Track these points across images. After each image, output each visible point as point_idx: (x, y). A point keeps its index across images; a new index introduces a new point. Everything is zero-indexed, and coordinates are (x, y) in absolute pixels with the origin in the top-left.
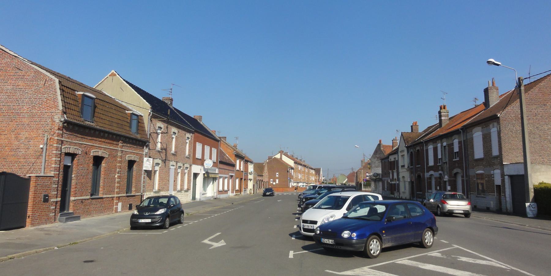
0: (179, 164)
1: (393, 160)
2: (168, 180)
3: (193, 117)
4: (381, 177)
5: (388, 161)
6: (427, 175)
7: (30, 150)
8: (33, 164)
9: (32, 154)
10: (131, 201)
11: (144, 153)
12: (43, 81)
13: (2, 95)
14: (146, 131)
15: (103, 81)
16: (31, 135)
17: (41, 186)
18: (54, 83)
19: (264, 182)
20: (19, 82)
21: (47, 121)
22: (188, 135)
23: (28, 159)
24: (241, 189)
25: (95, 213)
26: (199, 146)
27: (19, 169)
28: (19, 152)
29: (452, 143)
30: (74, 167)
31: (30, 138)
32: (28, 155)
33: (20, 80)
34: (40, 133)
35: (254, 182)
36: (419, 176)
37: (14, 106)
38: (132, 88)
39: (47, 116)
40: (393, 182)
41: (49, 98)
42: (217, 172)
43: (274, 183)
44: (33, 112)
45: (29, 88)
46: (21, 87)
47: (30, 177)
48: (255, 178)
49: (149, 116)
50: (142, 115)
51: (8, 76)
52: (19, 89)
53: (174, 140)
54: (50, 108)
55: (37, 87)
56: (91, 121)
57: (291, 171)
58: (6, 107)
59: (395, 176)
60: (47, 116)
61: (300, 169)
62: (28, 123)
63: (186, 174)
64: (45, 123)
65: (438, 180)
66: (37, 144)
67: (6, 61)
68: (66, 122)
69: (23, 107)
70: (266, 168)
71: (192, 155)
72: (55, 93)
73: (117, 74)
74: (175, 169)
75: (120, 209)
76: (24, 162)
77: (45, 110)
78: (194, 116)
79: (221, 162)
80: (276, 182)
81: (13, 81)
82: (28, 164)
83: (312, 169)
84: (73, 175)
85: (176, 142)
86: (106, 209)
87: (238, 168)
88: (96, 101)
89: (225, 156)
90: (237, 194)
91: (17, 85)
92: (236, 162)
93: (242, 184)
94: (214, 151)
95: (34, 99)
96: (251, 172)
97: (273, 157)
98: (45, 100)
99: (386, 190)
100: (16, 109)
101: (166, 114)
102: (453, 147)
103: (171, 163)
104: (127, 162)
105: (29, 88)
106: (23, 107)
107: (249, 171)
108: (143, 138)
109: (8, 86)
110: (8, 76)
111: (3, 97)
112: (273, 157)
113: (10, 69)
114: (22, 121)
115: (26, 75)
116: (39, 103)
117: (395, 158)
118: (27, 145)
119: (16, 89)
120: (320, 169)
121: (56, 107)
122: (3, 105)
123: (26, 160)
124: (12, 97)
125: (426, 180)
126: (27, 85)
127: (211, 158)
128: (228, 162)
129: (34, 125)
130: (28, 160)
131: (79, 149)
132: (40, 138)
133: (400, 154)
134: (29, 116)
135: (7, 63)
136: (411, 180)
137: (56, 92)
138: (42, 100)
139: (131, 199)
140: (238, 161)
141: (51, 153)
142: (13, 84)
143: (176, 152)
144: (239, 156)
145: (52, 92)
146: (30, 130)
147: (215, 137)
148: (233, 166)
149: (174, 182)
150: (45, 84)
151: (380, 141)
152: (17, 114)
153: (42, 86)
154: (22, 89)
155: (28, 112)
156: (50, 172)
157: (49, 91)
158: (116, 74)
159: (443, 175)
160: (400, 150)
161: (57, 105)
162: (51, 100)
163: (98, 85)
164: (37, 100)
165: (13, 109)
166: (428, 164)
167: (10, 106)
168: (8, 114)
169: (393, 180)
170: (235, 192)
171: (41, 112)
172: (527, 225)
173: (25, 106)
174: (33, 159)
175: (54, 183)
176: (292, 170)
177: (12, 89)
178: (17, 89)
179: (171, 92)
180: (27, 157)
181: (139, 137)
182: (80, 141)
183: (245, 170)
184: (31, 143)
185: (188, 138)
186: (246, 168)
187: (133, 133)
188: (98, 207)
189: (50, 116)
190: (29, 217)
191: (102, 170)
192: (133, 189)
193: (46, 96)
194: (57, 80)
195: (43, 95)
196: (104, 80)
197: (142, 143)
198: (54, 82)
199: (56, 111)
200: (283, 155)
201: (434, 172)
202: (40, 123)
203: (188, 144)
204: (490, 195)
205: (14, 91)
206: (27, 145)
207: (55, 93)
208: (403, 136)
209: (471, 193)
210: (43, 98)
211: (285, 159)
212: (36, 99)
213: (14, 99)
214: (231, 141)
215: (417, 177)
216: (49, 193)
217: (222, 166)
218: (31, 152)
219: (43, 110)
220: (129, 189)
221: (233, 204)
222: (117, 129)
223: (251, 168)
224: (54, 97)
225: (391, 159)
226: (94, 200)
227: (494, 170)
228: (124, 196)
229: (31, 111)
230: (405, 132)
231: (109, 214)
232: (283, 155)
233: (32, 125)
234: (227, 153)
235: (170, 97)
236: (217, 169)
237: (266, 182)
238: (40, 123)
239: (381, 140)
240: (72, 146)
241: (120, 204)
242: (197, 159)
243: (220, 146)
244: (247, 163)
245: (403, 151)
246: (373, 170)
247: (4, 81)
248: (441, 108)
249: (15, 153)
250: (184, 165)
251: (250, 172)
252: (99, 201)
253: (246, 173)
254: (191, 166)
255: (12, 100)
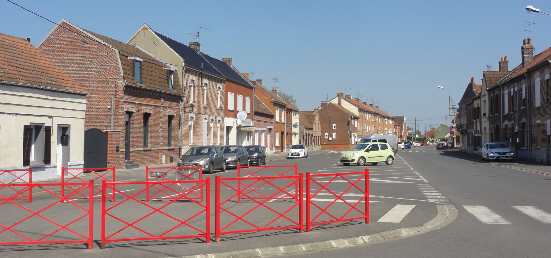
0: (212, 117)
1: (476, 106)
2: (202, 135)
3: (221, 60)
4: (465, 129)
5: (473, 107)
6: (503, 125)
7: (100, 110)
8: (104, 121)
9: (102, 113)
10: (174, 154)
11: (180, 108)
12: (105, 52)
13: (73, 65)
14: (180, 86)
15: (135, 36)
16: (100, 97)
17: (115, 139)
18: (115, 53)
19: (315, 137)
20: (86, 53)
21: (111, 86)
22: (219, 85)
23: (99, 117)
24: (282, 146)
25: (147, 163)
26: (231, 96)
27: (93, 125)
28: (91, 112)
29: (521, 88)
30: (131, 123)
31: (99, 100)
32: (99, 114)
33: (87, 52)
34: (107, 96)
35: (300, 137)
36: (497, 127)
37: (84, 73)
38: (165, 42)
39: (112, 81)
40: (477, 135)
41: (112, 66)
42: (252, 125)
43: (330, 139)
44: (100, 79)
45: (95, 59)
46: (88, 57)
47: (107, 132)
48: (301, 132)
49: (183, 70)
50: (177, 69)
51: (77, 48)
52: (87, 59)
53: (206, 91)
54: (113, 75)
55: (102, 57)
56: (140, 82)
57: (354, 122)
58: (77, 75)
59: (479, 129)
60: (112, 81)
61: (367, 119)
62: (97, 88)
63: (219, 129)
64: (110, 88)
65: (511, 131)
66: (106, 105)
67: (74, 35)
68: (127, 87)
69: (91, 75)
70: (317, 119)
71: (224, 107)
72: (116, 62)
73: (148, 28)
74: (208, 122)
75: (164, 161)
76: (96, 120)
77: (109, 76)
78: (223, 59)
79: (256, 113)
80: (332, 137)
81: (81, 52)
82: (100, 121)
83: (389, 118)
84: (131, 130)
85: (207, 94)
86: (154, 160)
87: (277, 119)
88: (143, 63)
89: (261, 105)
90: (277, 151)
91: (85, 56)
92: (275, 112)
93: (283, 139)
94: (248, 100)
95: (100, 67)
96: (296, 124)
97: (328, 103)
98: (109, 68)
99: (471, 145)
100: (86, 76)
101: (198, 67)
102: (521, 93)
103: (204, 116)
104: (167, 116)
105: (95, 59)
106: (91, 75)
107: (293, 122)
108: (180, 94)
109: (77, 56)
110: (77, 48)
111: (74, 66)
112: (328, 103)
113: (78, 42)
114: (92, 86)
115: (91, 47)
116: (104, 71)
117: (478, 104)
118: (98, 106)
119: (84, 59)
120: (404, 117)
121: (119, 74)
122: (74, 73)
123: (98, 118)
124: (82, 66)
125: (502, 132)
126: (93, 56)
127: (244, 109)
128: (265, 112)
129: (102, 89)
130: (100, 118)
131: (135, 107)
132: (107, 100)
133: (483, 99)
134: (96, 82)
135: (75, 37)
136: (491, 132)
137: (118, 61)
138: (107, 68)
139: (172, 152)
140: (277, 112)
141: (117, 112)
142: (81, 55)
143: (207, 104)
144: (278, 105)
145: (114, 61)
146: (99, 93)
147: (248, 83)
148: (272, 117)
149: (208, 136)
150: (107, 54)
151: (472, 80)
152: (87, 80)
153: (106, 56)
154: (89, 59)
155: (96, 79)
156: (118, 128)
157: (112, 61)
158: (147, 28)
159: (514, 125)
160: (482, 94)
161: (119, 72)
162: (114, 68)
163: (131, 40)
164: (102, 68)
165: (84, 76)
166: (504, 112)
167: (81, 73)
168: (79, 81)
169: (476, 132)
170: (274, 148)
171: (107, 79)
172: (532, 171)
173: (93, 73)
174: (103, 117)
175: (121, 136)
176: (356, 122)
177: (81, 59)
178: (85, 59)
179: (198, 36)
180: (98, 116)
181: (175, 92)
182: (134, 101)
183: (287, 121)
184: (100, 104)
185: (220, 88)
186: (289, 119)
187: (170, 90)
188: (149, 158)
189: (114, 81)
190: (109, 162)
191: (149, 125)
192: (173, 143)
193: (109, 64)
194: (117, 51)
195: (107, 64)
196: (137, 34)
197: (178, 99)
198: (115, 52)
199: (118, 77)
200: (342, 99)
201: (508, 122)
202: (106, 88)
203: (219, 95)
204: (544, 146)
205: (83, 61)
206: (98, 106)
207: (116, 62)
208: (485, 76)
209: (533, 145)
210: (107, 67)
211: (346, 105)
212: (101, 67)
213: (83, 68)
214: (268, 85)
215: (495, 128)
216: (119, 145)
217: (257, 117)
218: (101, 111)
219: (108, 77)
220: (169, 144)
221: (271, 161)
222: (158, 87)
223: (295, 119)
224: (116, 65)
225: (475, 105)
226: (145, 152)
227: (546, 120)
228: (166, 149)
229: (98, 77)
230: (492, 71)
231: (157, 165)
232: (342, 99)
233: (100, 89)
234: (263, 101)
235: (197, 41)
236: (252, 121)
237: (317, 137)
238: (106, 88)
239: (473, 78)
240: (130, 106)
241: (164, 156)
242: (230, 111)
243: (255, 93)
244: (289, 113)
245: (484, 95)
246: (462, 118)
247: (73, 52)
248: (524, 44)
249: (88, 113)
250: (216, 118)
251: (294, 124)
252: (149, 153)
253: (289, 125)
254: (223, 119)
255: (82, 69)
